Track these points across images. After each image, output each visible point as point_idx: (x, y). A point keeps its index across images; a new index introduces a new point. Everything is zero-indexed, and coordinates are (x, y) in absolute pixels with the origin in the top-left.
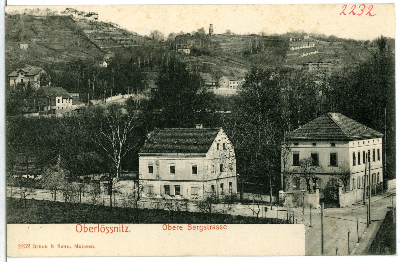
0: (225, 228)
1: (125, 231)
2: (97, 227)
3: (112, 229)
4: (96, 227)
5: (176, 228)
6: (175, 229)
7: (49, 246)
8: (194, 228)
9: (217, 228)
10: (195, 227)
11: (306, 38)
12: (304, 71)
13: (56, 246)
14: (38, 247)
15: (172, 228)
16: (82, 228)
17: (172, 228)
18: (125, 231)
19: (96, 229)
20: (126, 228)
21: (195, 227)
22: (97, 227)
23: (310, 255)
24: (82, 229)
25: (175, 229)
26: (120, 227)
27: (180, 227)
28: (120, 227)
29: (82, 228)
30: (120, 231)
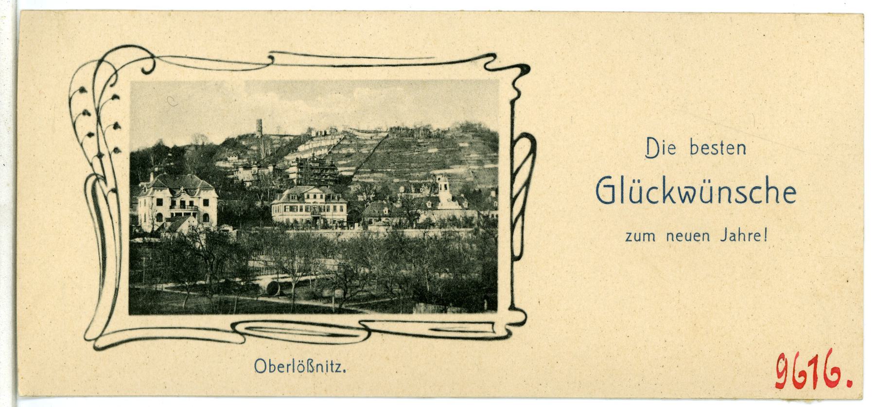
0: (672, 151)
1: (336, 371)
2: (290, 365)
3: (716, 149)
4: (289, 364)
5: (736, 150)
6: (283, 372)
8: (281, 369)
9: (715, 152)
10: (699, 236)
11: (269, 265)
12: (275, 267)
15: (277, 367)
16: (266, 366)
17: (781, 197)
18: (336, 371)
19: (289, 367)
20: (338, 366)
21: (699, 236)
22: (290, 365)
23: (862, 383)
24: (658, 151)
25: (283, 372)
26: (327, 365)
27: (755, 236)
28: (327, 365)
29: (266, 366)
30: (644, 240)
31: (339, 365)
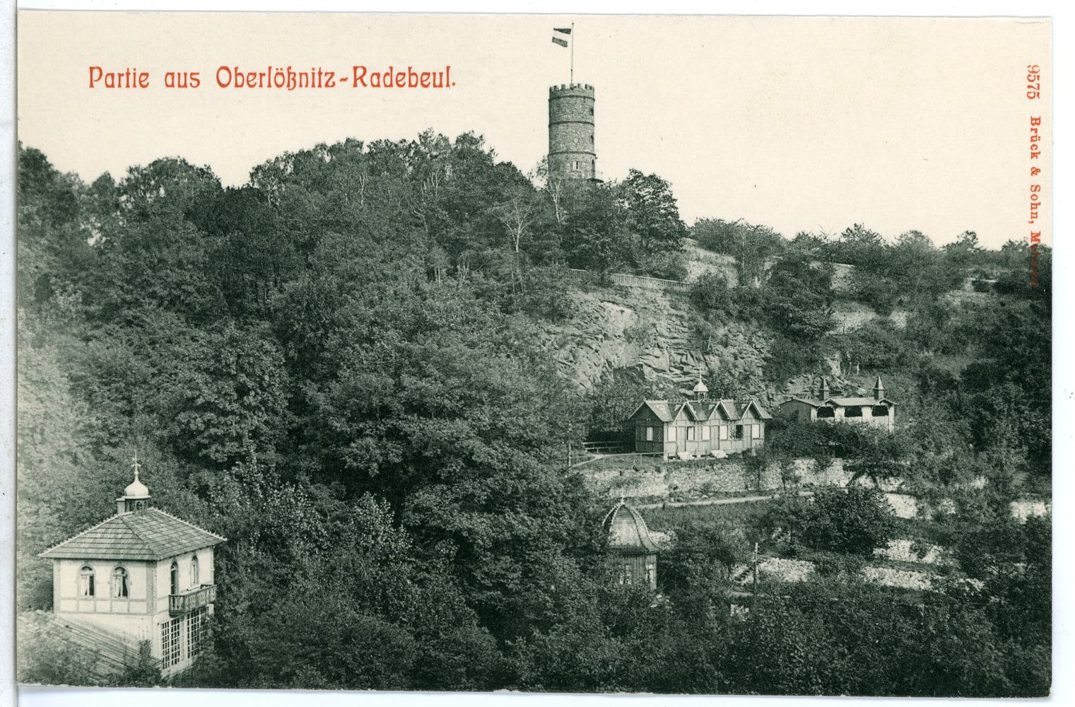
7: (1035, 163)
13: (1036, 180)
14: (1033, 134)
31: (333, 74)
